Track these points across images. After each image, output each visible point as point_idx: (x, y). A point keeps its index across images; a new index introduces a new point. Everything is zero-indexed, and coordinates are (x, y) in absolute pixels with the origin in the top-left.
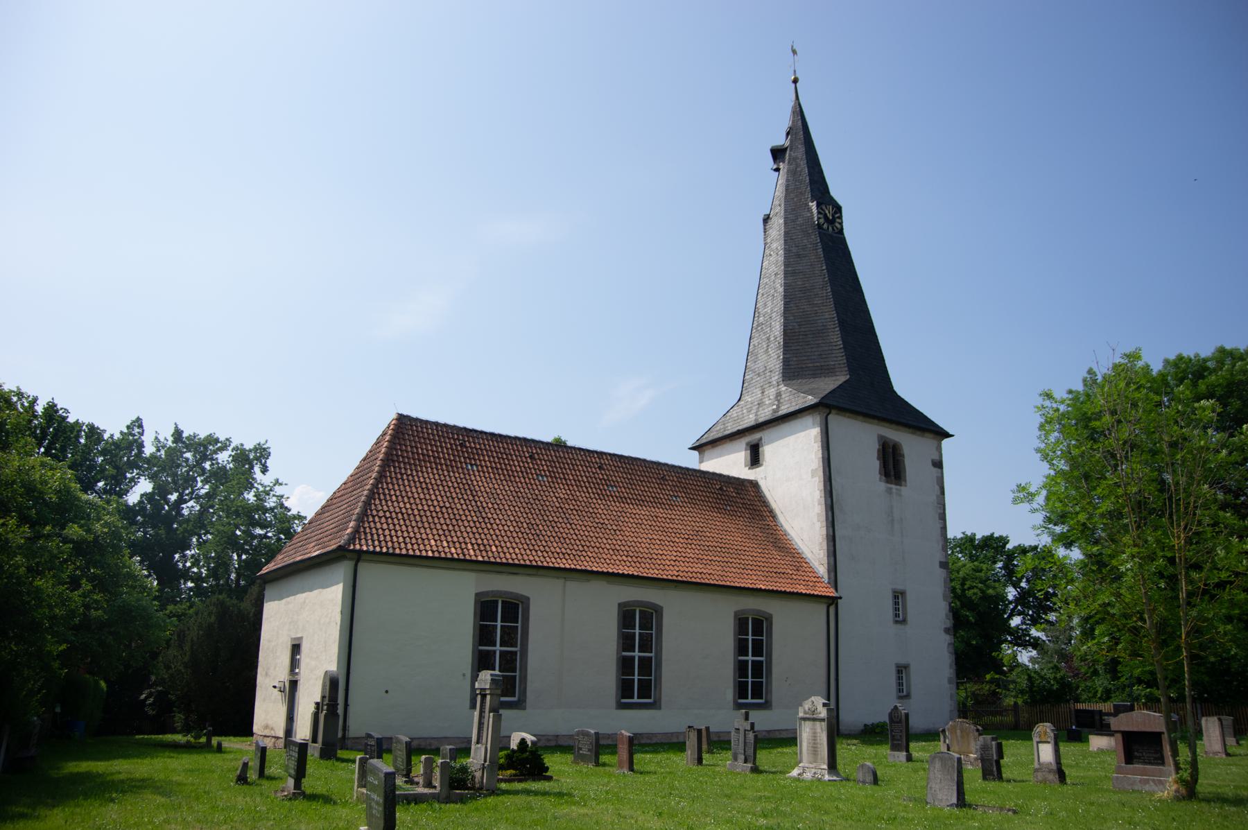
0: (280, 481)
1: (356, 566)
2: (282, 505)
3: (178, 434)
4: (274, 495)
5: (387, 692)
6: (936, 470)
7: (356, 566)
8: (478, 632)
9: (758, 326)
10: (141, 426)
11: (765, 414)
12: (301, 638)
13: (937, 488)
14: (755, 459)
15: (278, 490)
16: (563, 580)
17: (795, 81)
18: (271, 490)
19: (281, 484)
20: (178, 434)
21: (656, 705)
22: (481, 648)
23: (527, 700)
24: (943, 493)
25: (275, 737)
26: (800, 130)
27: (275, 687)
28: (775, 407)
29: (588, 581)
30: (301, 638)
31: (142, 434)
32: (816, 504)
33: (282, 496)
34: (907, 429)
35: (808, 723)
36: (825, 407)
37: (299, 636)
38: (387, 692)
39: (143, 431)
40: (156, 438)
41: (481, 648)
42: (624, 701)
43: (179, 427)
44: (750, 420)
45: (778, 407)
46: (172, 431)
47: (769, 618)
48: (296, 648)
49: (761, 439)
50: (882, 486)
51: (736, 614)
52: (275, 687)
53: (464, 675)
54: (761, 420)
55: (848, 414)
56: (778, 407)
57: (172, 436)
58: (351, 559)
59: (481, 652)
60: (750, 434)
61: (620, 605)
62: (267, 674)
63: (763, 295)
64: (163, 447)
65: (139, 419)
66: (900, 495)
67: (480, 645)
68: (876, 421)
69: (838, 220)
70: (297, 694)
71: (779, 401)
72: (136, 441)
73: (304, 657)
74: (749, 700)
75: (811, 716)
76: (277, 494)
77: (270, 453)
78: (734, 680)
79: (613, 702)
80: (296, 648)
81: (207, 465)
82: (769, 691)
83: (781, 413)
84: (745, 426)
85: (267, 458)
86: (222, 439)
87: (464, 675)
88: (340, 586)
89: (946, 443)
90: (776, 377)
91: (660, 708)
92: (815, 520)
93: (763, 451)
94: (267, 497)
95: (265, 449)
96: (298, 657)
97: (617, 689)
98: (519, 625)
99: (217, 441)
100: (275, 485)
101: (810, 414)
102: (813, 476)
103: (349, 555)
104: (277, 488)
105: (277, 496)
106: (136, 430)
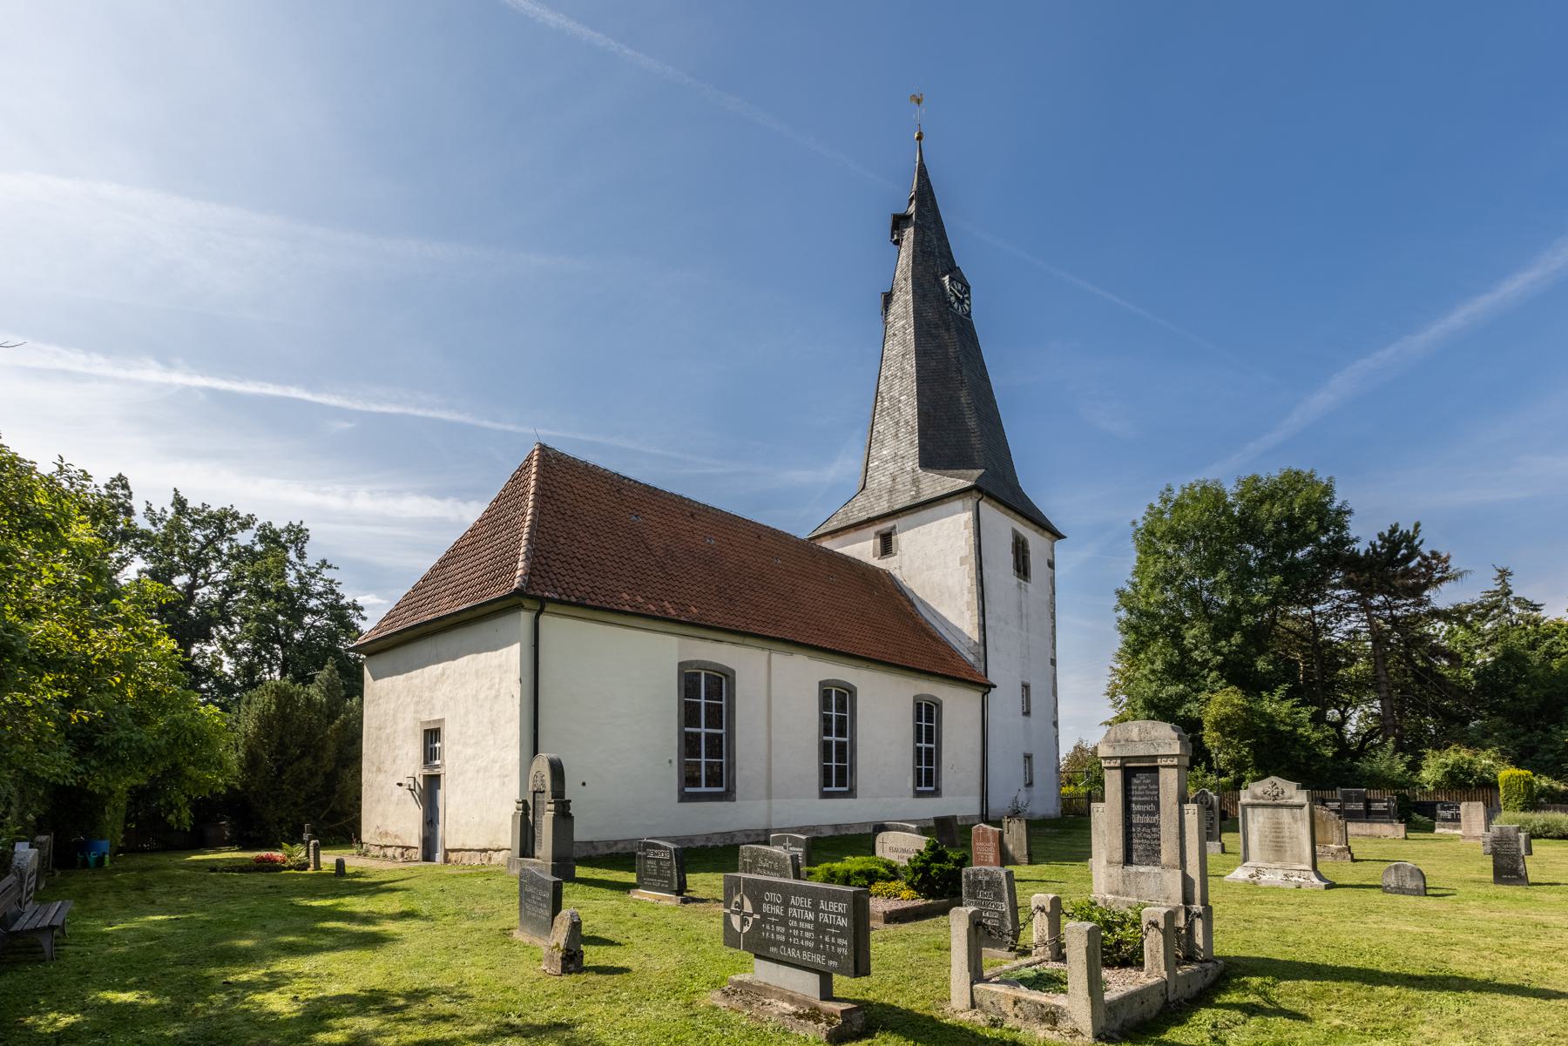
0: (328, 563)
1: (537, 618)
2: (333, 592)
3: (180, 504)
4: (321, 579)
5: (584, 784)
6: (1049, 569)
7: (537, 618)
8: (683, 709)
9: (882, 411)
10: (125, 487)
11: (903, 500)
12: (442, 721)
13: (1050, 587)
14: (887, 545)
15: (327, 574)
16: (767, 653)
17: (919, 138)
18: (317, 572)
19: (330, 567)
20: (180, 504)
21: (851, 793)
22: (687, 729)
23: (737, 791)
24: (1054, 593)
25: (403, 847)
26: (925, 194)
27: (400, 785)
28: (913, 493)
29: (792, 654)
30: (442, 721)
31: (130, 496)
32: (966, 592)
33: (332, 581)
34: (1033, 526)
35: (1259, 811)
36: (979, 491)
37: (436, 717)
38: (584, 784)
39: (131, 493)
40: (149, 509)
41: (687, 729)
42: (688, 790)
43: (181, 494)
44: (882, 507)
45: (918, 492)
46: (171, 499)
47: (939, 705)
48: (432, 736)
49: (894, 527)
50: (1015, 580)
51: (915, 698)
52: (400, 785)
53: (670, 762)
54: (897, 507)
55: (993, 503)
56: (918, 492)
57: (172, 505)
58: (529, 610)
59: (687, 734)
60: (881, 523)
61: (820, 683)
62: (379, 770)
63: (886, 378)
64: (161, 520)
65: (121, 477)
66: (1026, 591)
67: (686, 726)
68: (1013, 513)
69: (967, 301)
70: (440, 793)
71: (917, 486)
72: (122, 505)
73: (449, 746)
74: (834, 788)
75: (1270, 802)
76: (325, 578)
77: (308, 536)
78: (914, 767)
79: (816, 792)
80: (432, 736)
81: (225, 547)
82: (938, 779)
83: (922, 499)
84: (875, 514)
85: (305, 542)
86: (243, 514)
87: (670, 762)
88: (516, 649)
89: (1058, 543)
90: (912, 463)
91: (855, 797)
92: (964, 608)
93: (897, 540)
94: (313, 581)
95: (301, 531)
96: (438, 745)
97: (820, 775)
98: (724, 702)
99: (235, 516)
100: (322, 567)
101: (960, 498)
102: (961, 564)
103: (526, 603)
104: (324, 571)
105: (325, 581)
106: (119, 492)
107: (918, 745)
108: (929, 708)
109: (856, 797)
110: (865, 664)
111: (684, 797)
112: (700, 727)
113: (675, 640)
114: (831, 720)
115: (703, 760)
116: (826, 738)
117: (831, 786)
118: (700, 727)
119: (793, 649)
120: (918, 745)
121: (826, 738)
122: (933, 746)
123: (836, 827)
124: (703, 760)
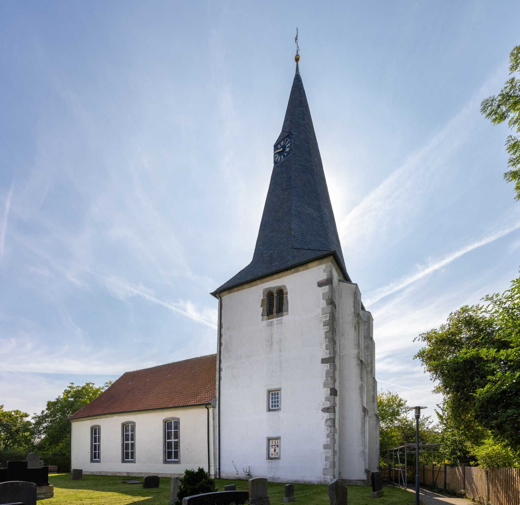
21: (178, 462)
53: (89, 452)
107: (99, 443)
108: (95, 430)
109: (90, 463)
110: (138, 413)
111: (165, 462)
112: (174, 439)
113: (89, 421)
114: (129, 436)
115: (173, 450)
116: (177, 440)
117: (129, 459)
118: (174, 439)
119: (112, 415)
120: (99, 443)
121: (177, 440)
122: (94, 444)
123: (128, 473)
124: (173, 450)
